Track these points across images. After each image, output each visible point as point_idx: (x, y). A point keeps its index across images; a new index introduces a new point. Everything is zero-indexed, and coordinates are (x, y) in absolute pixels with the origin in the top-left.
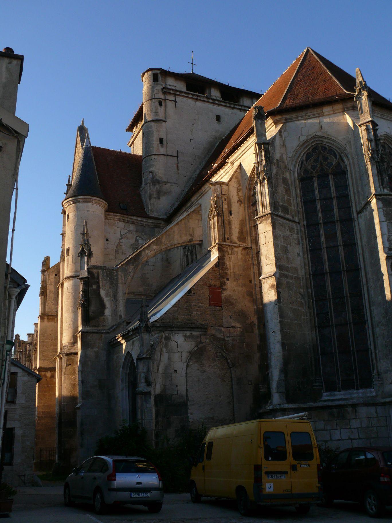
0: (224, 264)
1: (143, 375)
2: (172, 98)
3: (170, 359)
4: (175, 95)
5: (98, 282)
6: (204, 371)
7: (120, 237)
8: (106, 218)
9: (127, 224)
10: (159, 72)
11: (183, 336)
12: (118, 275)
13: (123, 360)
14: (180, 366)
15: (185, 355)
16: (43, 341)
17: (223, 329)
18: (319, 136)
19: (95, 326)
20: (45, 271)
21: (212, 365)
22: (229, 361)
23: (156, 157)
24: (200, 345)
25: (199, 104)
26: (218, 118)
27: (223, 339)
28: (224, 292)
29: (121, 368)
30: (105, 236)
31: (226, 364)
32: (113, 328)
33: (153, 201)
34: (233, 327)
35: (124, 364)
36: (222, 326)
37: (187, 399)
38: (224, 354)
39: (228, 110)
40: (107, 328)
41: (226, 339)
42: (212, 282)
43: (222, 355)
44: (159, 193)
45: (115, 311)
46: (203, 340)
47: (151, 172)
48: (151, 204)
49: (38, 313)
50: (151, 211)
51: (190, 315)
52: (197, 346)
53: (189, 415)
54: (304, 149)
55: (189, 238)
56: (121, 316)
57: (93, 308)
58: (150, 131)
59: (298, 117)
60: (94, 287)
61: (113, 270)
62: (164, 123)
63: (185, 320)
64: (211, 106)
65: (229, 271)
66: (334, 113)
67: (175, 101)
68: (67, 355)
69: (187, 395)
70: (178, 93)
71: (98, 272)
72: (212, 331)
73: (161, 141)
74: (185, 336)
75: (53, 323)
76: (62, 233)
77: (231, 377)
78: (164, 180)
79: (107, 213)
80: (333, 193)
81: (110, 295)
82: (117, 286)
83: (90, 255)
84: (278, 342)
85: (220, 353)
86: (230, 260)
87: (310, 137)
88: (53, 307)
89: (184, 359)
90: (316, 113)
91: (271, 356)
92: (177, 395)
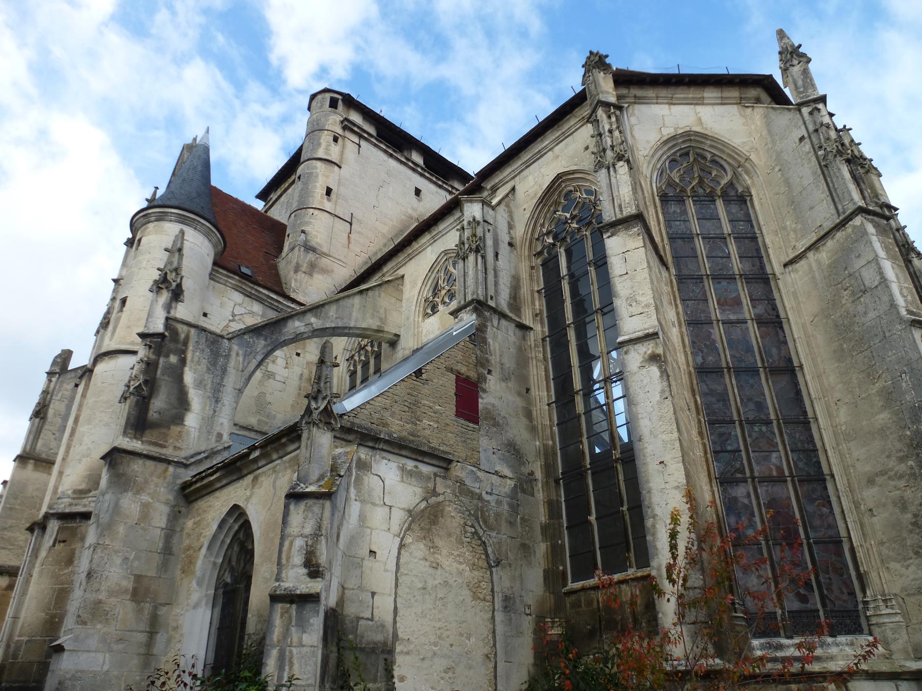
0: (484, 341)
1: (299, 543)
2: (356, 139)
3: (362, 518)
4: (361, 137)
5: (184, 352)
6: (436, 566)
7: (231, 318)
8: (212, 277)
9: (247, 299)
10: (340, 97)
11: (399, 467)
12: (230, 350)
13: (215, 527)
14: (384, 541)
15: (398, 517)
16: (11, 509)
17: (479, 474)
18: (697, 134)
19: (156, 444)
20: (55, 373)
21: (456, 553)
22: (490, 550)
23: (316, 212)
24: (433, 500)
25: (393, 163)
26: (418, 192)
27: (480, 497)
28: (484, 396)
29: (204, 551)
30: (203, 308)
31: (483, 557)
32: (199, 457)
33: (300, 275)
34: (496, 473)
35: (215, 537)
36: (477, 465)
37: (395, 636)
38: (481, 532)
39: (432, 187)
40: (183, 454)
41: (486, 497)
42: (463, 370)
43: (476, 533)
44: (313, 268)
45: (209, 422)
46: (440, 489)
47: (303, 232)
48: (296, 280)
49: (17, 442)
50: (294, 291)
51: (416, 424)
52: (425, 499)
53: (396, 680)
54: (670, 149)
55: (378, 323)
56: (220, 436)
57: (158, 404)
58: (311, 173)
59: (657, 97)
60: (173, 359)
61: (222, 337)
62: (336, 168)
63: (404, 434)
64: (410, 172)
65: (493, 357)
66: (722, 104)
67: (360, 146)
68: (64, 517)
69: (395, 622)
70: (366, 135)
71: (189, 332)
72: (458, 471)
73: (329, 192)
74: (402, 469)
75: (45, 475)
76: (115, 277)
77: (492, 590)
78: (325, 250)
79: (216, 268)
80: (727, 228)
81: (205, 386)
82: (224, 371)
83: (177, 295)
84: (677, 487)
85: (472, 526)
86: (495, 337)
87: (680, 131)
88: (53, 444)
89: (395, 528)
90: (691, 96)
91: (654, 526)
92: (372, 620)
